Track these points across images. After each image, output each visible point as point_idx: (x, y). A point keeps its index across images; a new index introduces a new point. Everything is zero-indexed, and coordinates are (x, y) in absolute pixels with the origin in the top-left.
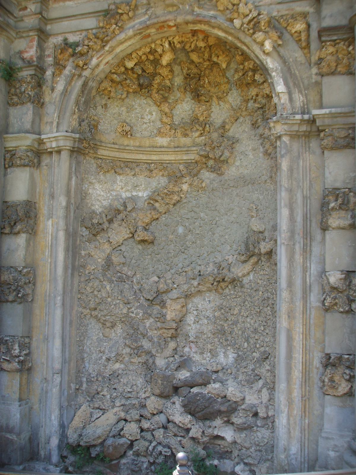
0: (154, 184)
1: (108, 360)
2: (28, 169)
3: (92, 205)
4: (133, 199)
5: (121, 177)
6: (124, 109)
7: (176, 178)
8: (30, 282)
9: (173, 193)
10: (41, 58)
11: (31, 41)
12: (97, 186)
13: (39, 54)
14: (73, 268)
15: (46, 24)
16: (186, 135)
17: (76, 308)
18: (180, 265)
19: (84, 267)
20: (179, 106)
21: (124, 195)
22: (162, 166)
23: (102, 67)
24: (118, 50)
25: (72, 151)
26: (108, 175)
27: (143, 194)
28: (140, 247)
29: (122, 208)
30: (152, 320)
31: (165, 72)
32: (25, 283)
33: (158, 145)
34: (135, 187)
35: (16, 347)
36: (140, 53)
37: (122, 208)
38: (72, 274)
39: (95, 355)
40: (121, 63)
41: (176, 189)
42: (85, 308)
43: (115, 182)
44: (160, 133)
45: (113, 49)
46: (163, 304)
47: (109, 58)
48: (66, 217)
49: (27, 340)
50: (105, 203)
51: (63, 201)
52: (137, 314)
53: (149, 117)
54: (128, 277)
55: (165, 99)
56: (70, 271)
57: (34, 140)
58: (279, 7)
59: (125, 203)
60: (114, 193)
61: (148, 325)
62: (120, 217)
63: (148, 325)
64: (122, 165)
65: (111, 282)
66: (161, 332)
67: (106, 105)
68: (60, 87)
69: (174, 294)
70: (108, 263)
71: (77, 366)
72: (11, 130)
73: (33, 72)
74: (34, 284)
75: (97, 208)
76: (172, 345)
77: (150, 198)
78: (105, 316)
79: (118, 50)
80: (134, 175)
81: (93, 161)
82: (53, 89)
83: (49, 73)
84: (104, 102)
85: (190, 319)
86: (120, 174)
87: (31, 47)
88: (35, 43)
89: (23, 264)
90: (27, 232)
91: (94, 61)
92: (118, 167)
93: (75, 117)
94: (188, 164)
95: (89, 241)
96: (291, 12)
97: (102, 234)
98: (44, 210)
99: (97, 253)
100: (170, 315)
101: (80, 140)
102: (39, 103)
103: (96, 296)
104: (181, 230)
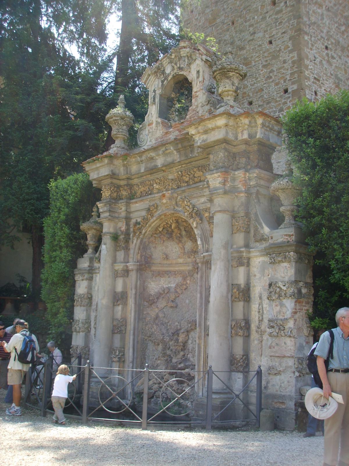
0: (177, 281)
1: (156, 359)
2: (122, 278)
3: (150, 292)
4: (169, 289)
5: (163, 278)
6: (164, 247)
7: (185, 279)
8: (123, 325)
9: (184, 284)
10: (128, 229)
11: (124, 223)
12: (152, 283)
13: (126, 228)
14: (139, 319)
15: (130, 214)
16: (189, 257)
17: (141, 336)
18: (187, 318)
19: (145, 318)
20: (187, 244)
21: (165, 287)
22: (180, 272)
23: (147, 233)
24: (153, 225)
25: (137, 270)
26: (157, 278)
27: (173, 285)
28: (171, 309)
29: (162, 292)
30: (173, 342)
31: (176, 230)
32: (121, 326)
33: (179, 262)
34: (169, 282)
35: (118, 352)
36: (162, 225)
37: (162, 292)
38: (138, 322)
39: (151, 357)
40: (157, 229)
41: (185, 283)
42: (145, 336)
43: (160, 281)
44: (179, 257)
45: (150, 226)
46: (178, 335)
47: (150, 229)
48: (135, 298)
49: (122, 349)
50: (156, 290)
51: (134, 291)
52: (167, 339)
53: (175, 250)
54: (166, 323)
55: (180, 241)
56: (137, 320)
57: (124, 266)
58: (202, 205)
59: (164, 290)
60: (160, 286)
61: (171, 344)
62: (162, 296)
63: (171, 344)
64: (163, 273)
65: (157, 325)
66: (177, 347)
67: (155, 247)
68: (135, 242)
69: (182, 331)
70: (157, 317)
71: (141, 361)
72: (117, 261)
73: (124, 237)
74: (126, 326)
75: (152, 293)
76: (182, 353)
77: (175, 288)
78: (154, 340)
79: (153, 225)
80: (169, 277)
81: (150, 272)
82: (133, 243)
83: (131, 235)
84: (154, 246)
85: (190, 342)
86: (162, 277)
87: (123, 226)
88: (125, 224)
89: (120, 318)
90: (122, 304)
91: (144, 231)
92: (160, 274)
93: (139, 255)
94: (189, 271)
95: (148, 307)
96: (206, 207)
97: (154, 304)
98: (129, 295)
99: (152, 312)
100: (181, 339)
101: (140, 265)
102: (127, 249)
103: (150, 331)
104: (187, 301)
